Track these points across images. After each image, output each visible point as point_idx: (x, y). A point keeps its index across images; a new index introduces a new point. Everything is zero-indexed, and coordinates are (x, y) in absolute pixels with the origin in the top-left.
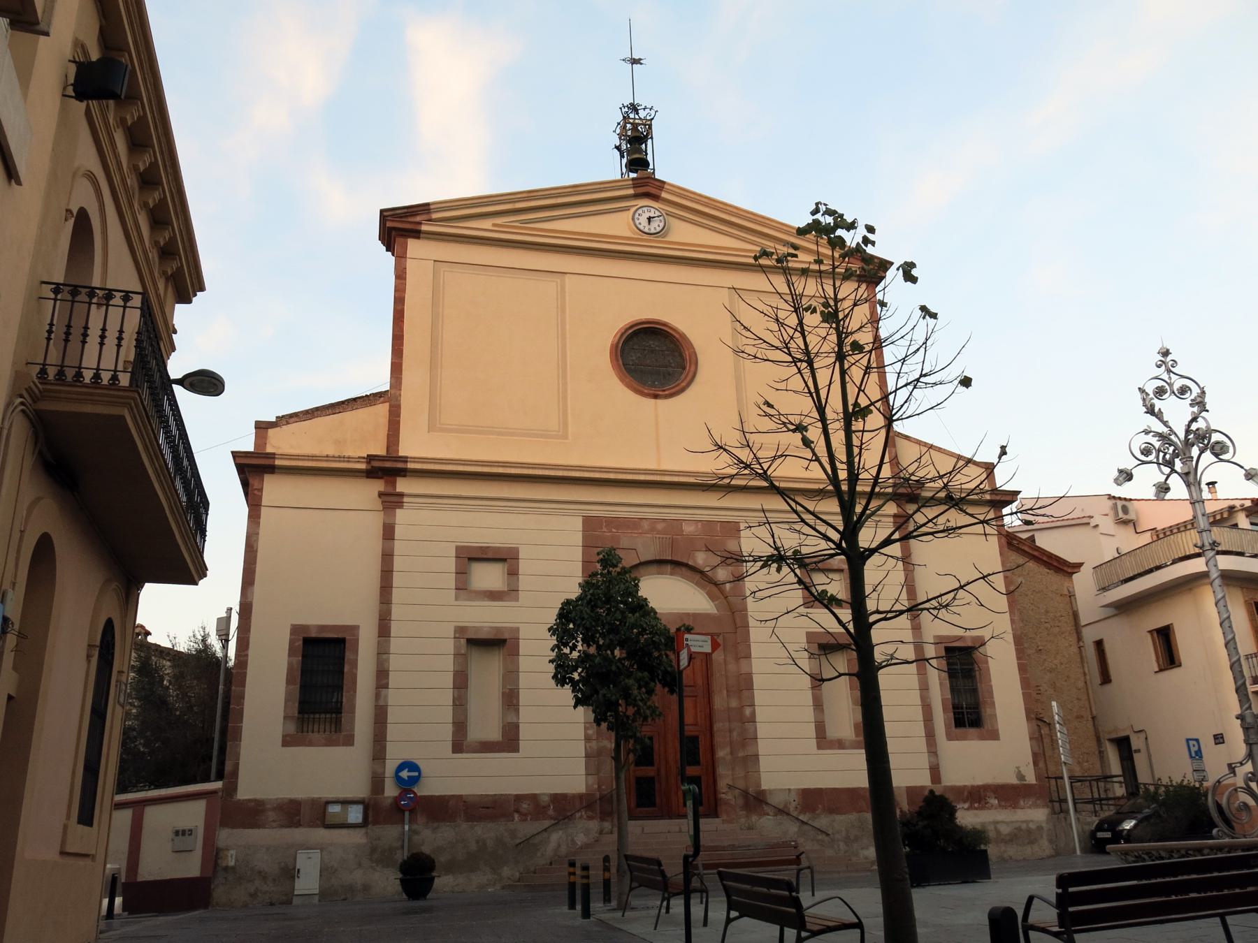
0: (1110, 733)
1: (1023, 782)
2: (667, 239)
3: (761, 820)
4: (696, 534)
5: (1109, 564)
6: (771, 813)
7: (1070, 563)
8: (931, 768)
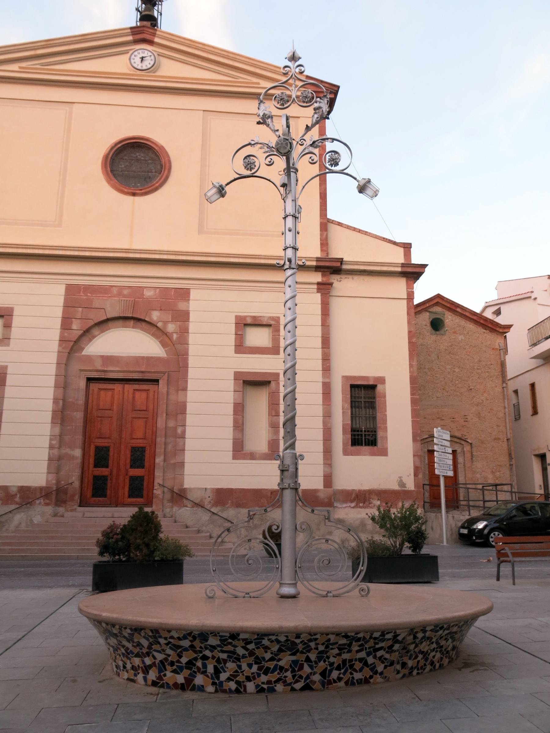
0: (534, 450)
1: (403, 489)
2: (158, 74)
3: (180, 511)
4: (154, 297)
5: (537, 326)
6: (189, 506)
7: (501, 325)
8: (325, 476)
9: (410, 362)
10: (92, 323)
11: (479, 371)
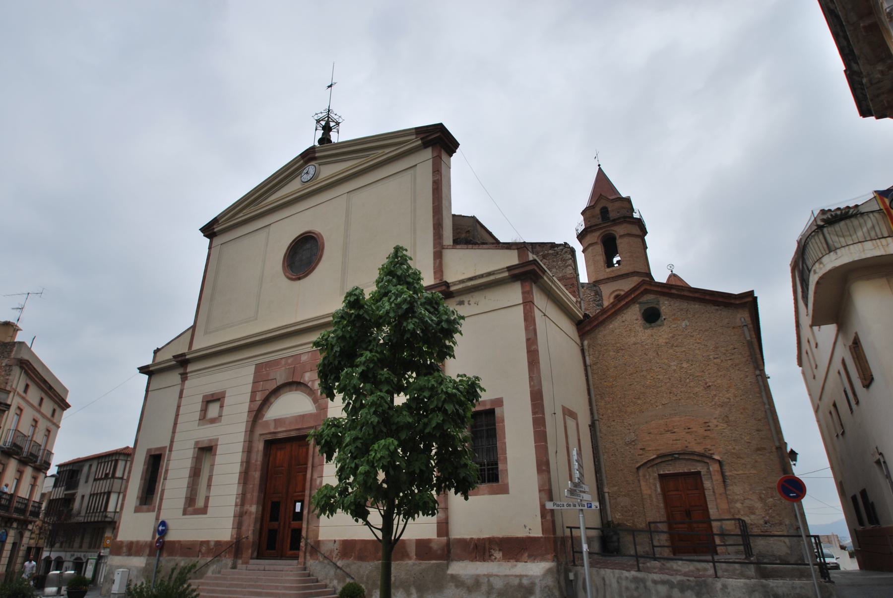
9: (529, 374)
10: (267, 392)
11: (718, 361)
